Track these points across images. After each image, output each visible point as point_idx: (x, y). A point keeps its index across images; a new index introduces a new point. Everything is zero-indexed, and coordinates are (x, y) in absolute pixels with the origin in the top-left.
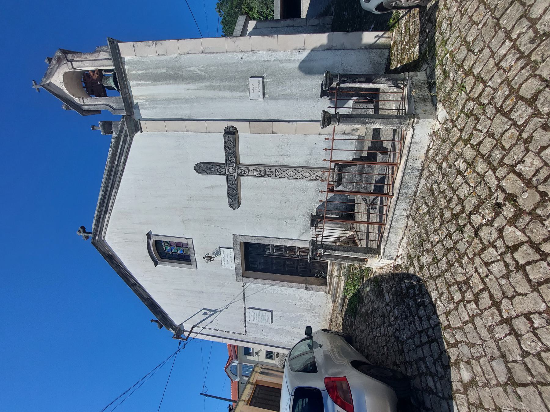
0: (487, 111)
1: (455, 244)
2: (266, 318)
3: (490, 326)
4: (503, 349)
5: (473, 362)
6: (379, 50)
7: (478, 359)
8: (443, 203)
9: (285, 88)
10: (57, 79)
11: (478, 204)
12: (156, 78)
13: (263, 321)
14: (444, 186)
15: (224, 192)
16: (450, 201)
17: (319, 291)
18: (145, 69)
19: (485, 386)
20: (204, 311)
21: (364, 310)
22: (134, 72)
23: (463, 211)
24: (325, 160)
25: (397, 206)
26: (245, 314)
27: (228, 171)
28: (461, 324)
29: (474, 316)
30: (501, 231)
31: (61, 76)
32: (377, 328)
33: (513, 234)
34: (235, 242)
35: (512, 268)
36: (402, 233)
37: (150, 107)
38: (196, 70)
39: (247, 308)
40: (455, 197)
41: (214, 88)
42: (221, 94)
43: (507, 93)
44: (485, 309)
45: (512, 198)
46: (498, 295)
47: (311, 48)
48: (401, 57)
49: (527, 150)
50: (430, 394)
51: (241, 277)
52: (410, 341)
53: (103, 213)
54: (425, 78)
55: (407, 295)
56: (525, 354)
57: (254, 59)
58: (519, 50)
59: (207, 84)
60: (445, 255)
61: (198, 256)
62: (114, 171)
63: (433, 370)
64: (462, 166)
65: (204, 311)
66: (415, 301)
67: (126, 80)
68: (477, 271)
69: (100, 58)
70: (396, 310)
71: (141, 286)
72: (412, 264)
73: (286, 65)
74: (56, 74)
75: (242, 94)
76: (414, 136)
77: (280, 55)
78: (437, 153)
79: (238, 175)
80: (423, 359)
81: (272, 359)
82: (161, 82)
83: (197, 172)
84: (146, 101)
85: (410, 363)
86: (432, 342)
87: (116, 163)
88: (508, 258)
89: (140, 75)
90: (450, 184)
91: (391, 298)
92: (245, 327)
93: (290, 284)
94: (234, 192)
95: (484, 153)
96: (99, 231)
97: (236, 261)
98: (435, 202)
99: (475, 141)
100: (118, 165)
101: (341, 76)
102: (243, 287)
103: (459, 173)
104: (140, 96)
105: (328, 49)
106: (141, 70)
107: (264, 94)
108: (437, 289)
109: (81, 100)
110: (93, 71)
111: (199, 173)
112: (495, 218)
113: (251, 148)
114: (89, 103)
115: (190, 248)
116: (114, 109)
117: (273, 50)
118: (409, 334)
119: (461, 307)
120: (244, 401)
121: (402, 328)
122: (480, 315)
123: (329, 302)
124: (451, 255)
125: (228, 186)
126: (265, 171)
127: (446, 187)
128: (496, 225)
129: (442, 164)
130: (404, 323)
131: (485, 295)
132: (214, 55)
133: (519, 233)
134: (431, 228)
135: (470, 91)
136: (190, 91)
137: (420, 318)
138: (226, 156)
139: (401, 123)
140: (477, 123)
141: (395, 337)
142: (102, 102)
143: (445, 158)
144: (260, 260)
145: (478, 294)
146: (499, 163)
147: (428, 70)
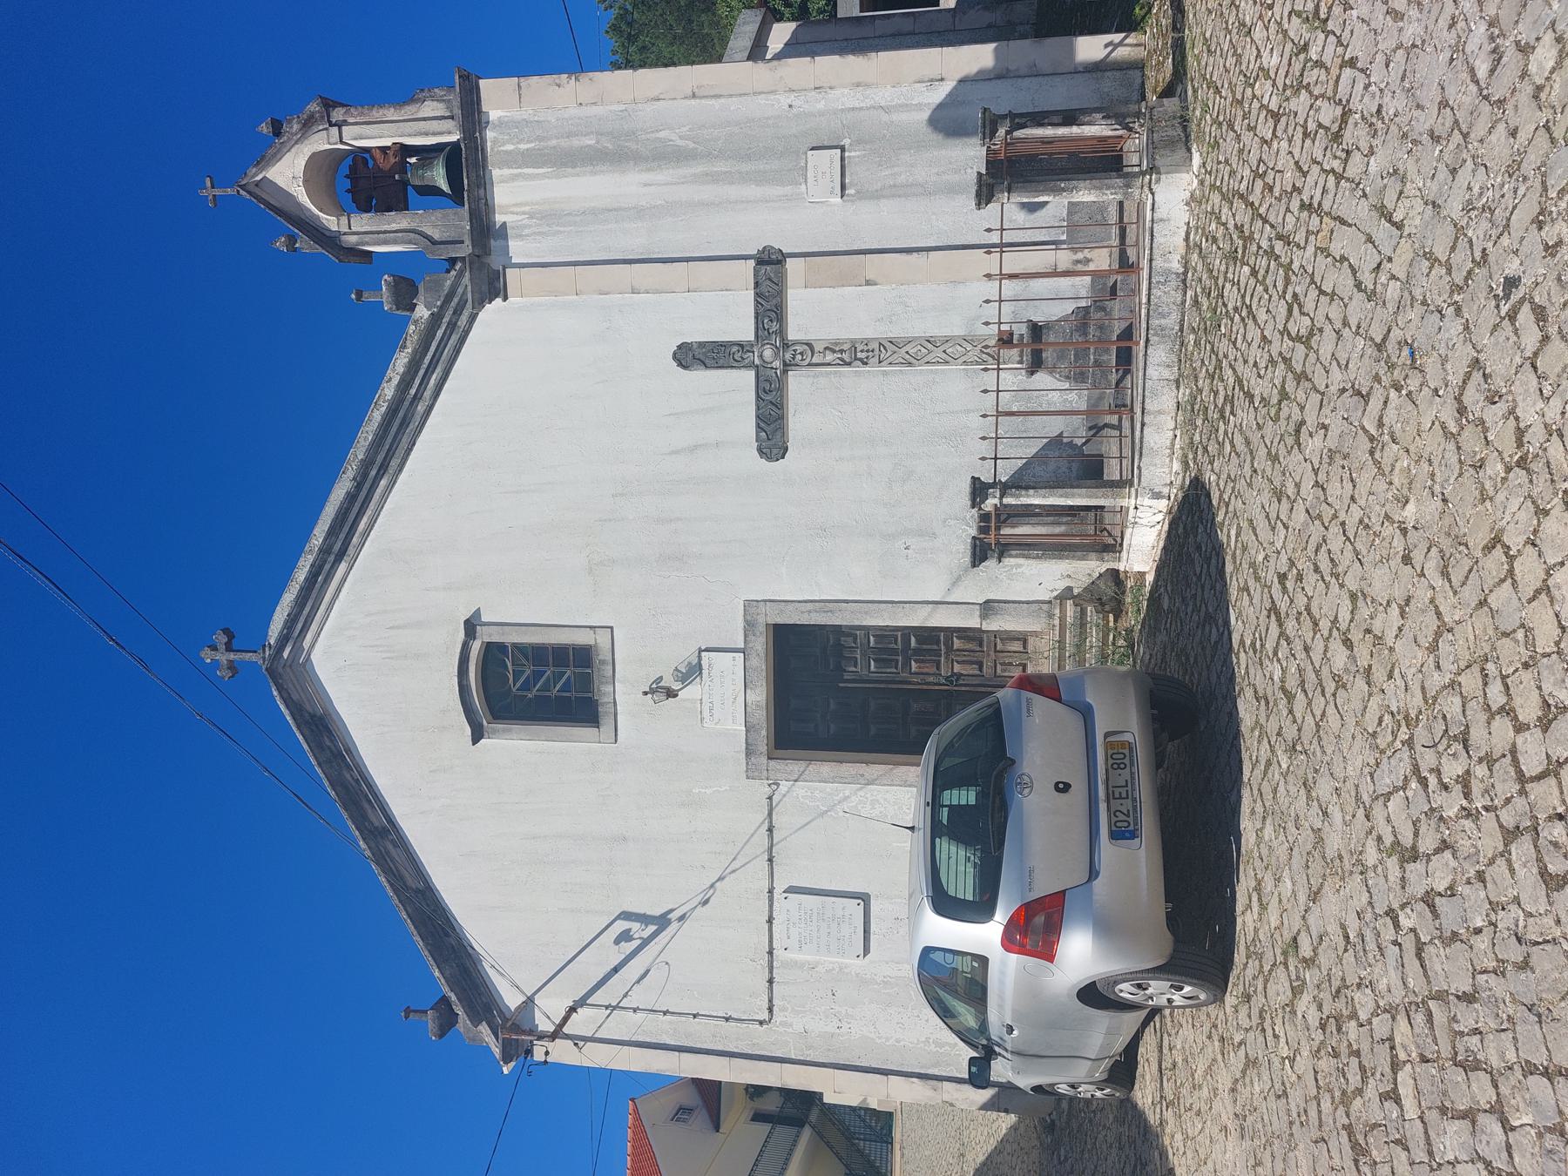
10: (288, 173)
12: (567, 160)
18: (540, 139)
20: (621, 926)
22: (510, 147)
25: (1150, 360)
26: (770, 921)
27: (761, 356)
31: (301, 163)
34: (749, 626)
39: (779, 889)
41: (715, 178)
47: (959, 76)
51: (764, 760)
53: (332, 558)
57: (821, 106)
59: (699, 169)
61: (624, 695)
62: (401, 414)
65: (621, 926)
67: (485, 167)
69: (420, 115)
71: (402, 843)
75: (788, 189)
77: (884, 95)
79: (785, 364)
83: (680, 365)
87: (413, 391)
89: (523, 154)
92: (771, 981)
94: (775, 412)
96: (299, 626)
97: (752, 697)
100: (417, 397)
101: (1012, 116)
102: (770, 798)
105: (999, 77)
107: (843, 187)
109: (344, 220)
110: (384, 149)
111: (685, 367)
113: (811, 311)
114: (359, 228)
115: (603, 662)
116: (434, 243)
117: (867, 85)
125: (758, 396)
132: (722, 100)
138: (756, 318)
139: (1128, 186)
142: (404, 224)
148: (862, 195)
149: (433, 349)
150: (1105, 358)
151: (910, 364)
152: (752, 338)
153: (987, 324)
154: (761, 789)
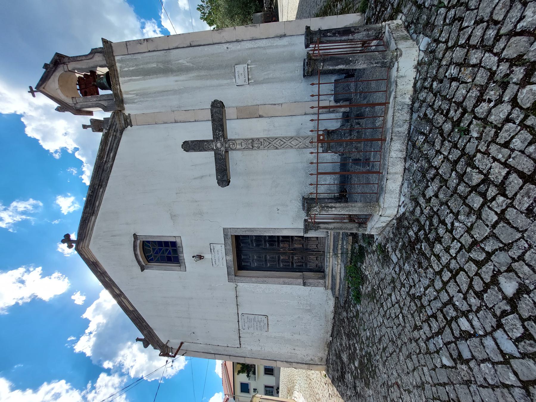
2: (262, 324)
3: (527, 209)
5: (516, 265)
7: (521, 258)
9: (268, 72)
11: (481, 93)
12: (147, 73)
13: (259, 329)
17: (317, 286)
18: (137, 65)
22: (126, 69)
24: (312, 96)
26: (238, 321)
28: (489, 231)
29: (503, 211)
31: (57, 79)
34: (226, 236)
37: (140, 101)
38: (185, 62)
41: (200, 78)
42: (209, 82)
44: (516, 194)
50: (466, 340)
51: (233, 277)
52: (431, 289)
55: (418, 240)
57: (239, 47)
61: (187, 255)
67: (118, 78)
70: (406, 265)
72: (418, 204)
73: (269, 51)
74: (52, 77)
75: (229, 81)
76: (399, 69)
80: (450, 301)
81: (272, 395)
82: (151, 77)
83: (185, 142)
84: (137, 95)
86: (457, 273)
87: (105, 160)
90: (444, 98)
92: (240, 337)
104: (131, 91)
106: (133, 67)
112: (503, 93)
113: (235, 128)
115: (179, 247)
118: (427, 282)
121: (416, 280)
122: (511, 205)
123: (330, 299)
127: (440, 103)
136: (179, 83)
144: (253, 254)
145: (503, 183)
148: (257, 83)
149: (109, 144)
150: (359, 145)
151: (277, 148)
152: (211, 138)
154: (233, 285)
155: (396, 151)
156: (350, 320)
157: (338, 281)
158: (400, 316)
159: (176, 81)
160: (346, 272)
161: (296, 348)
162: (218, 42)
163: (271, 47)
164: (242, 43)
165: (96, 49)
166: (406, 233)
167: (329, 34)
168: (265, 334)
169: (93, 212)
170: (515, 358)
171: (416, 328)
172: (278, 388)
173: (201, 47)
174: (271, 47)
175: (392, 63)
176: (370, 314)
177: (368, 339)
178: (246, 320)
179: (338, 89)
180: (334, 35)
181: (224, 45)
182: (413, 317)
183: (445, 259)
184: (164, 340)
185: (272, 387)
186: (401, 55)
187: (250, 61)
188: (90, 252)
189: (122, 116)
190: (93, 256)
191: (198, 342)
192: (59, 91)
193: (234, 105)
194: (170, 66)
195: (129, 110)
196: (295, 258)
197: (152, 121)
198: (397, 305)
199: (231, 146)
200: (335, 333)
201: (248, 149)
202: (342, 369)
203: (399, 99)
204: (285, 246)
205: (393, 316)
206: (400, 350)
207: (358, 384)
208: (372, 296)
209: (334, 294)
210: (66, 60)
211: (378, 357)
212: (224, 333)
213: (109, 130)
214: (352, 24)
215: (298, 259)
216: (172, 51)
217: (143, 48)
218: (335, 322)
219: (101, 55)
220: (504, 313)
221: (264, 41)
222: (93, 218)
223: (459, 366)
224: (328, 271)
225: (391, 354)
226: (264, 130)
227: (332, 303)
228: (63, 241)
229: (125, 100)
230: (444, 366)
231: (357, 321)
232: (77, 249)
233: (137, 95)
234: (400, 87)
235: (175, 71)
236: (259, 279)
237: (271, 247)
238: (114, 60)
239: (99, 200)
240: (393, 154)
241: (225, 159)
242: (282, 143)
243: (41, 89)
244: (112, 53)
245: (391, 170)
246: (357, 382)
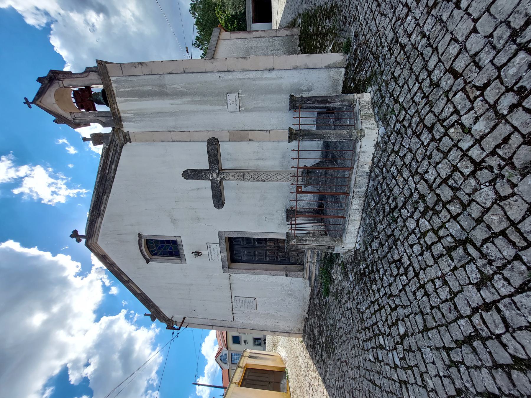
0: (408, 132)
1: (393, 231)
2: (251, 304)
4: (422, 306)
6: (336, 69)
7: (408, 316)
8: (384, 200)
9: (258, 101)
13: (249, 307)
14: (384, 187)
15: (209, 193)
16: (388, 199)
17: (298, 277)
18: (132, 87)
19: (412, 335)
21: (335, 290)
22: (122, 90)
23: (396, 207)
30: (418, 221)
31: (53, 94)
32: (345, 303)
33: (424, 224)
34: (220, 237)
35: (424, 248)
36: (359, 224)
37: (138, 120)
38: (179, 87)
40: (391, 195)
41: (195, 102)
43: (418, 120)
45: (422, 197)
46: (417, 267)
48: (353, 77)
49: (430, 164)
54: (370, 99)
55: (364, 274)
56: (432, 308)
57: (230, 77)
58: (423, 91)
60: (387, 241)
61: (187, 251)
63: (383, 331)
64: (395, 173)
66: (370, 278)
67: (115, 97)
68: (405, 252)
72: (366, 249)
73: (258, 82)
74: (48, 92)
75: (221, 107)
78: (379, 161)
82: (147, 98)
84: (134, 114)
85: (368, 328)
87: (107, 171)
88: (422, 242)
91: (354, 278)
93: (272, 272)
95: (407, 163)
98: (380, 199)
99: (402, 153)
103: (394, 177)
106: (129, 88)
108: (383, 268)
112: (414, 212)
113: (231, 154)
119: (398, 280)
120: (235, 383)
121: (362, 301)
123: (307, 286)
124: (391, 240)
126: (244, 175)
128: (415, 217)
129: (382, 169)
130: (363, 297)
131: (411, 268)
133: (427, 223)
134: (377, 219)
135: (398, 115)
136: (174, 105)
137: (373, 291)
140: (402, 140)
141: (357, 309)
143: (385, 165)
144: (242, 251)
146: (415, 171)
147: (372, 93)
148: (247, 110)
149: (110, 158)
151: (265, 181)
153: (293, 167)
154: (227, 275)
155: (356, 206)
156: (321, 306)
157: (314, 275)
158: (351, 319)
159: (172, 104)
160: (319, 270)
161: (279, 321)
162: (210, 71)
163: (261, 79)
164: (234, 73)
165: (91, 68)
166: (359, 265)
167: (309, 102)
168: (255, 311)
169: (99, 215)
170: (399, 367)
171: (358, 331)
172: (265, 340)
173: (194, 74)
174: (261, 79)
175: (356, 141)
176: (334, 309)
177: (331, 325)
178: (238, 302)
179: (319, 122)
180: (314, 103)
181: (216, 74)
182: (358, 323)
183: (377, 296)
184: (169, 315)
185: (260, 339)
186: (364, 136)
187: (240, 90)
188: (99, 247)
189: (121, 134)
190: (101, 250)
191: (198, 317)
192: (56, 106)
193: (226, 129)
194: (166, 90)
195: (127, 127)
196: (280, 254)
197: (151, 138)
198: (350, 311)
199: (225, 177)
200: (310, 312)
201: (241, 180)
202: (314, 340)
203: (361, 168)
204: (271, 244)
205: (347, 316)
206: (349, 342)
207: (323, 354)
208: (336, 296)
209: (310, 285)
210: (60, 76)
211: (337, 341)
212: (220, 310)
213: (110, 145)
214: (336, 63)
215: (282, 255)
216: (166, 75)
217: (138, 70)
218: (310, 304)
219: (96, 74)
220: (398, 343)
221: (254, 73)
222: (100, 219)
223: (376, 363)
224: (307, 266)
225: (344, 342)
226: (254, 152)
227: (309, 289)
228: (72, 236)
229: (123, 119)
230: (370, 360)
231: (326, 309)
232: (87, 244)
233: (134, 114)
234: (362, 159)
235: (170, 95)
236: (250, 271)
237: (260, 245)
238: (110, 80)
239: (104, 204)
240: (354, 207)
241: (220, 187)
242: (269, 177)
243: (38, 102)
244: (108, 73)
245: (352, 218)
246: (323, 352)
